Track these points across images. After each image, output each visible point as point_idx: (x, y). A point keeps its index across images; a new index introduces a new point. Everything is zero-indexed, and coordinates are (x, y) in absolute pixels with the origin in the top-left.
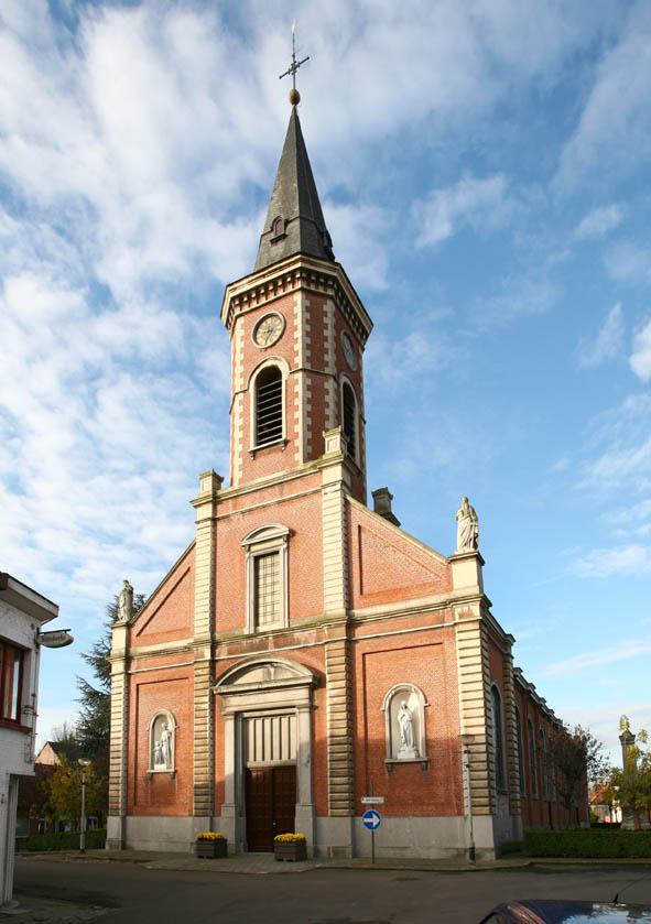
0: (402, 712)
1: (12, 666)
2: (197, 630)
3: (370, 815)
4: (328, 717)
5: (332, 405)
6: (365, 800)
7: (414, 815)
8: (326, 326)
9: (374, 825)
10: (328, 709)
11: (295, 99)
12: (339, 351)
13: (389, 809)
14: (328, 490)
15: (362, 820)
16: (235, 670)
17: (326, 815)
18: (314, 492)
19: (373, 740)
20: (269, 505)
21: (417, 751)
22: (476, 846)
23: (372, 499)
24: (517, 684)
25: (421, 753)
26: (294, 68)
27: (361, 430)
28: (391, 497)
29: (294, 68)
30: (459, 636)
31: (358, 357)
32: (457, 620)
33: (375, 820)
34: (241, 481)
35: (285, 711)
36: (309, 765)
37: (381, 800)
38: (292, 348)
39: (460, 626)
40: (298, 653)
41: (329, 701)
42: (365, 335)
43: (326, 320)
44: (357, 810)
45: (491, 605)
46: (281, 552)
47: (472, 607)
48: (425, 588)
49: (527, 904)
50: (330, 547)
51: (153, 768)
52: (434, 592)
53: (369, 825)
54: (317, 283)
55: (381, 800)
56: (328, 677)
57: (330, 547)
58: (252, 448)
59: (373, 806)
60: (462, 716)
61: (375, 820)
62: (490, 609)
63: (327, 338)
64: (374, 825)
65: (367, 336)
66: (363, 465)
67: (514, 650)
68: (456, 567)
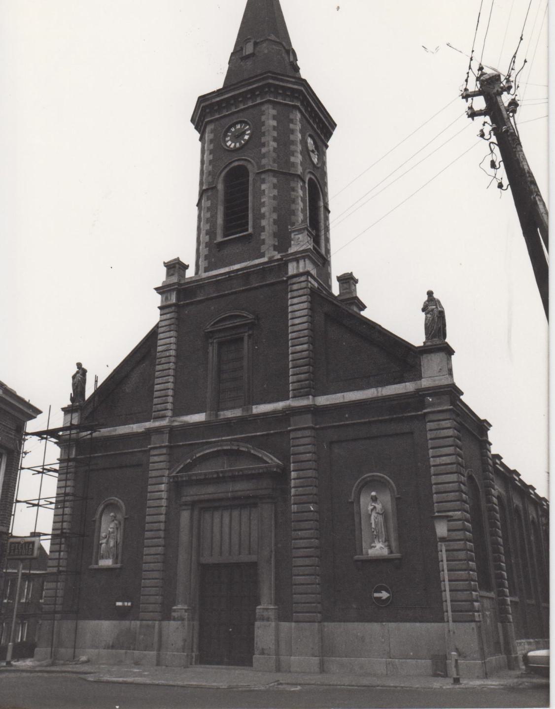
1: (484, 425)
8: (293, 132)
12: (306, 152)
19: (206, 419)
24: (497, 471)
27: (327, 219)
28: (356, 281)
30: (430, 426)
31: (322, 155)
42: (328, 135)
45: (462, 393)
46: (246, 338)
50: (156, 459)
51: (97, 563)
57: (156, 459)
58: (220, 239)
62: (462, 397)
63: (264, 228)
65: (331, 134)
66: (328, 251)
67: (492, 435)
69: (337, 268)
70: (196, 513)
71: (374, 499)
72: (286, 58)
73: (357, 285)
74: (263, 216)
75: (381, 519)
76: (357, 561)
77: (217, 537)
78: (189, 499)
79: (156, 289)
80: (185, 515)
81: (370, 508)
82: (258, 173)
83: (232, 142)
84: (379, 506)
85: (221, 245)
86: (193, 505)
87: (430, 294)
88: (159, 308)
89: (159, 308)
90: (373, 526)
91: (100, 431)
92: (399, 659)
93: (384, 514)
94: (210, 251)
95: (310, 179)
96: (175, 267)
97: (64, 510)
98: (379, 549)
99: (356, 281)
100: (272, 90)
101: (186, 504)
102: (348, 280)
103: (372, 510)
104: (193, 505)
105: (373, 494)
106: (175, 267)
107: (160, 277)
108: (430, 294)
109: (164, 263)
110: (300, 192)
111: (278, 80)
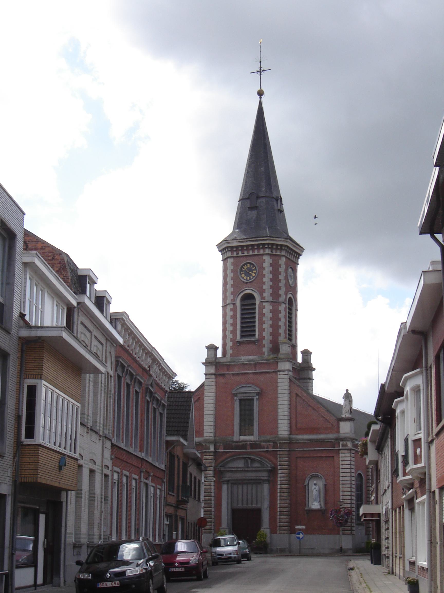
0: (314, 487)
2: (205, 435)
3: (299, 534)
4: (279, 487)
5: (283, 320)
6: (297, 527)
7: (318, 534)
9: (301, 538)
10: (279, 483)
11: (260, 94)
13: (305, 532)
14: (281, 373)
15: (293, 536)
16: (153, 430)
17: (276, 533)
18: (274, 372)
20: (248, 373)
21: (321, 505)
22: (343, 548)
23: (301, 355)
25: (322, 506)
26: (261, 71)
29: (261, 71)
30: (341, 455)
32: (341, 447)
33: (301, 536)
34: (231, 355)
35: (258, 482)
36: (268, 509)
37: (304, 527)
38: (262, 287)
39: (342, 450)
40: (263, 454)
41: (279, 479)
43: (280, 270)
44: (293, 531)
47: (347, 443)
48: (326, 430)
49: (319, 487)
52: (331, 432)
53: (299, 538)
54: (276, 249)
55: (304, 527)
56: (279, 467)
59: (300, 529)
60: (278, 518)
61: (301, 536)
64: (301, 538)
68: (342, 424)
69: (300, 348)
70: (230, 485)
71: (315, 485)
72: (275, 205)
73: (311, 355)
74: (264, 330)
75: (317, 493)
76: (306, 510)
77: (240, 497)
78: (226, 479)
79: (203, 363)
80: (225, 487)
81: (313, 488)
82: (261, 302)
83: (245, 275)
84: (317, 488)
85: (240, 343)
86: (228, 482)
87: (347, 390)
88: (204, 374)
89: (204, 374)
90: (314, 496)
91: (267, 509)
92: (154, 494)
93: (319, 491)
94: (233, 344)
95: (290, 298)
96: (212, 348)
97: (289, 537)
98: (315, 505)
99: (311, 353)
100: (270, 246)
101: (225, 481)
102: (306, 353)
103: (314, 489)
104: (228, 482)
105: (315, 482)
106: (212, 348)
107: (204, 355)
108: (347, 390)
109: (206, 347)
110: (282, 308)
111: (273, 240)
